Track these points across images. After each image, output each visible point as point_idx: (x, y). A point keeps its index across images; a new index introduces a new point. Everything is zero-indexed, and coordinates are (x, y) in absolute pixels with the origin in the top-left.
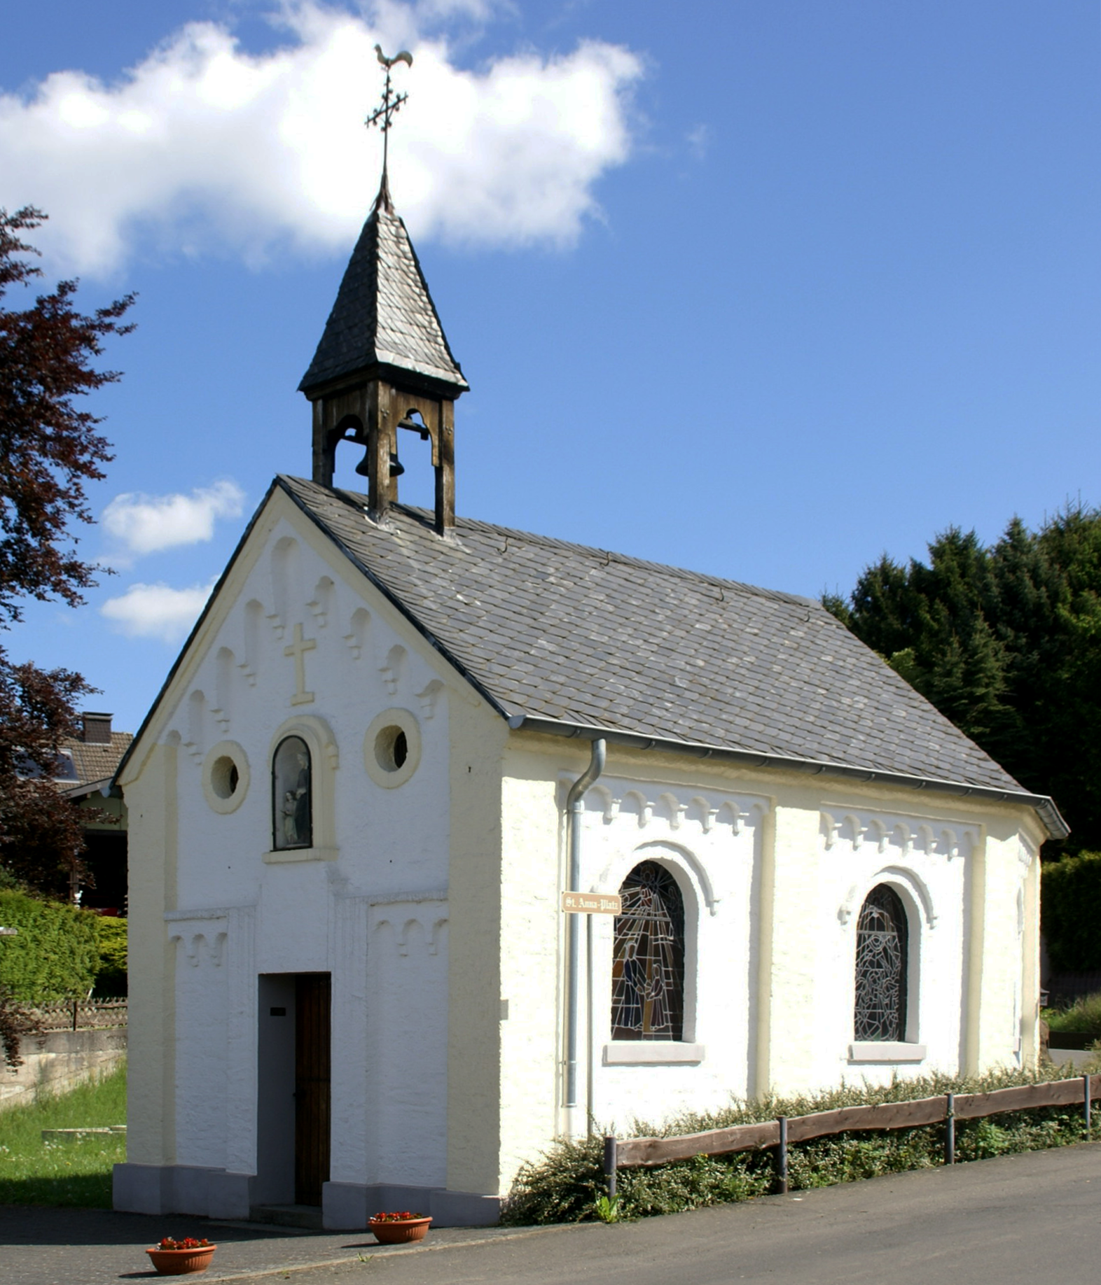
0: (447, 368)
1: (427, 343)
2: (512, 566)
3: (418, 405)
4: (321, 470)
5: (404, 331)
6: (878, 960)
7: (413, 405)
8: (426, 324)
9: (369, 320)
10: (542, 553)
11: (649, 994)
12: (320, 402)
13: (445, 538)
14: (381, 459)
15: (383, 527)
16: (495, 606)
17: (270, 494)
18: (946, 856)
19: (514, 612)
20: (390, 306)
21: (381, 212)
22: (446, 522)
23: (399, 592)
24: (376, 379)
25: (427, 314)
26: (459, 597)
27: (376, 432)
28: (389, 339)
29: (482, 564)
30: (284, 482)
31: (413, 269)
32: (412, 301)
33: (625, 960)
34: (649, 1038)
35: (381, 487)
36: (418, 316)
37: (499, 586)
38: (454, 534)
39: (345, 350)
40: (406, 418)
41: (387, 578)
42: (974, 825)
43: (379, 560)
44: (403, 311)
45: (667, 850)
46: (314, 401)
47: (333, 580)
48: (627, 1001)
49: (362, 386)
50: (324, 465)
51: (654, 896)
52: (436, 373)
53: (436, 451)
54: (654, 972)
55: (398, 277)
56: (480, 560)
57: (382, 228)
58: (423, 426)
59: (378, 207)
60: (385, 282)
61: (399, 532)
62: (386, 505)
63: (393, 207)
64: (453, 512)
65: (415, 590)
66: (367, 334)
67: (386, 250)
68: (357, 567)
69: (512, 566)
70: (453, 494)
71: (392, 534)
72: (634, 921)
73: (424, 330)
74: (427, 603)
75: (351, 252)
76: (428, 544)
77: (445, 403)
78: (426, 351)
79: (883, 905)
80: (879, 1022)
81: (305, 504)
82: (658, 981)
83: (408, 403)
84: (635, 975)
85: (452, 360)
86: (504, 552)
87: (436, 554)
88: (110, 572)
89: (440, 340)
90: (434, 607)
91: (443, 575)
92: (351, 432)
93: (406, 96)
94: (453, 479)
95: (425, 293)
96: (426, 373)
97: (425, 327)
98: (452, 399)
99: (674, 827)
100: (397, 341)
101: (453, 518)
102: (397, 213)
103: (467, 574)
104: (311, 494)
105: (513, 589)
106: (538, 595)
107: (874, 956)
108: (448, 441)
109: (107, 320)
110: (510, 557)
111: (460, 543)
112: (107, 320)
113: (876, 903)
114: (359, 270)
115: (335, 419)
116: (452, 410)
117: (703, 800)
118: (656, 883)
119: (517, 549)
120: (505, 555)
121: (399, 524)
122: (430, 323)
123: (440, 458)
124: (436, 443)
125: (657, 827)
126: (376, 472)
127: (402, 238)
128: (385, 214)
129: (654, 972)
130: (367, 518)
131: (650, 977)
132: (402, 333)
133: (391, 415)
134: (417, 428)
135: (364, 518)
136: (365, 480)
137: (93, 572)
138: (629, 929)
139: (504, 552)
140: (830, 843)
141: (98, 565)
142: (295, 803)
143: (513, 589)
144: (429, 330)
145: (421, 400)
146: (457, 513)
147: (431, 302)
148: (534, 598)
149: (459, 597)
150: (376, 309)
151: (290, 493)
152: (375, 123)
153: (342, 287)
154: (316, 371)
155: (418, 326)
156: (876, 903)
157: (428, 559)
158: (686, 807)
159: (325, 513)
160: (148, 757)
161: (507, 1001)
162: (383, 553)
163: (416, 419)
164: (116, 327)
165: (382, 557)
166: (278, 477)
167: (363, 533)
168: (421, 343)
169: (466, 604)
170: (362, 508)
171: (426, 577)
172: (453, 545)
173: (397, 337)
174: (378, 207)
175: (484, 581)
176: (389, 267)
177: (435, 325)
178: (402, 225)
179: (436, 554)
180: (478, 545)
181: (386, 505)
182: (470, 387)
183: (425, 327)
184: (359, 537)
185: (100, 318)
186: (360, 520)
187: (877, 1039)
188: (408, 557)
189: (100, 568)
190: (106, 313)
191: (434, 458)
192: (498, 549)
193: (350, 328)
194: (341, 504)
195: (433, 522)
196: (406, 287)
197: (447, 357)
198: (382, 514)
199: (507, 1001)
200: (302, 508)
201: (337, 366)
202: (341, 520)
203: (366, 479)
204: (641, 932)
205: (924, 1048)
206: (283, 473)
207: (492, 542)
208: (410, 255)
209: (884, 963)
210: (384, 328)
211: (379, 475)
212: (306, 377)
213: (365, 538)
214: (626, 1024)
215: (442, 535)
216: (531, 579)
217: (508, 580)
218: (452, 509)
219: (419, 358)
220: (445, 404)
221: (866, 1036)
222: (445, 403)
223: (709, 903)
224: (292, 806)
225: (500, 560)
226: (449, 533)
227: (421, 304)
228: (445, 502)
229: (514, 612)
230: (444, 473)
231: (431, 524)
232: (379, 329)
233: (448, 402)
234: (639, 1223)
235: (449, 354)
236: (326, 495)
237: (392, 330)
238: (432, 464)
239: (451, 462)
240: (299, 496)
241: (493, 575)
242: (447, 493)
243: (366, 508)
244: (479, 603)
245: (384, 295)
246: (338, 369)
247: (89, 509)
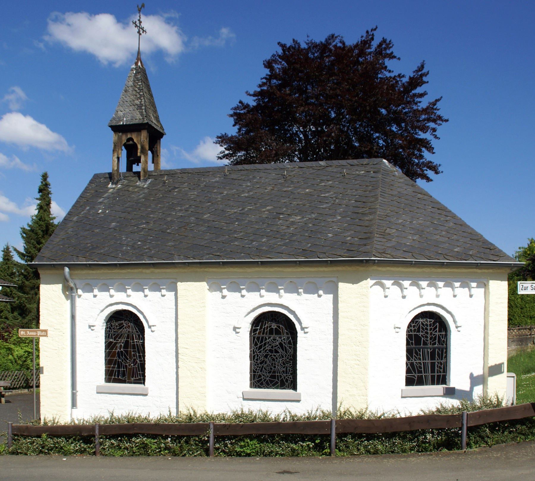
6: (275, 349)
11: (130, 365)
18: (316, 295)
33: (117, 351)
34: (130, 383)
42: (334, 277)
45: (435, 307)
48: (119, 367)
51: (131, 324)
54: (132, 355)
72: (122, 335)
79: (278, 321)
80: (278, 379)
82: (135, 360)
84: (122, 357)
99: (280, 297)
107: (272, 347)
113: (274, 321)
117: (468, 281)
118: (132, 319)
125: (120, 296)
129: (132, 355)
131: (130, 357)
138: (119, 338)
140: (455, 294)
156: (274, 321)
158: (225, 287)
161: (43, 367)
187: (277, 388)
199: (43, 367)
204: (125, 339)
205: (300, 394)
209: (280, 350)
214: (118, 376)
221: (269, 387)
223: (302, 329)
234: (107, 460)
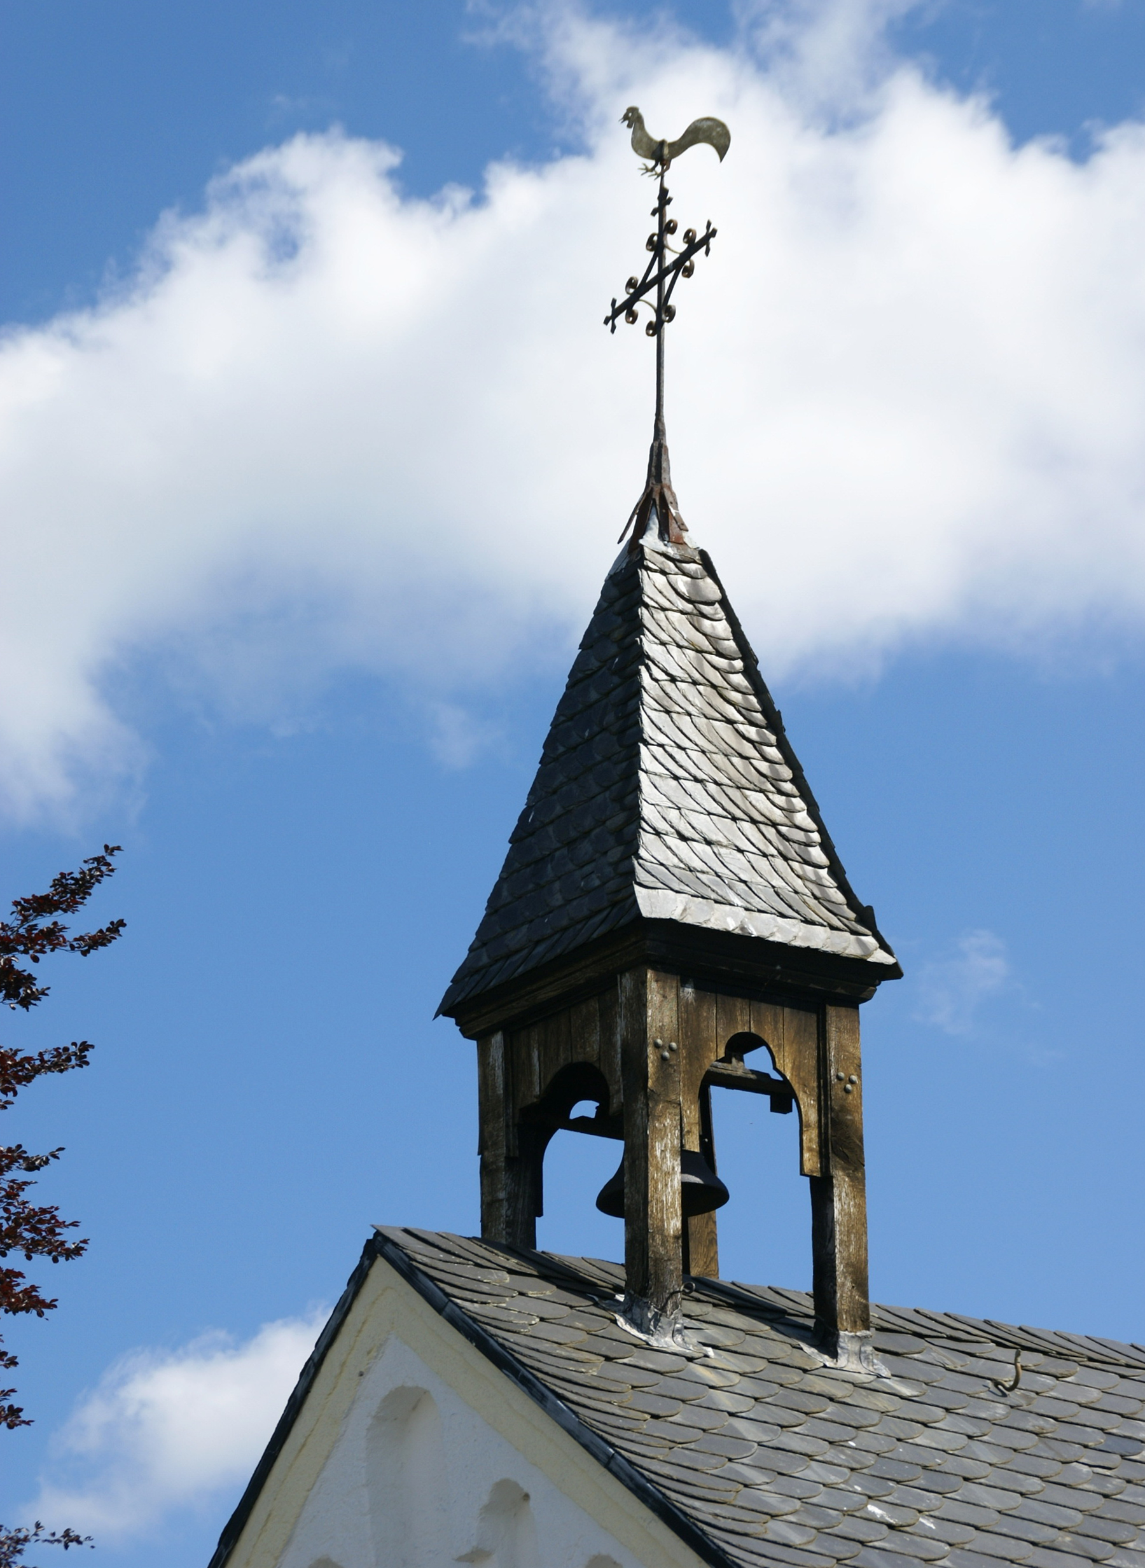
0: (835, 921)
1: (779, 862)
2: (1033, 1423)
3: (759, 1023)
4: (504, 1210)
5: (713, 836)
7: (744, 1024)
8: (778, 815)
9: (620, 818)
10: (1125, 1386)
12: (498, 1039)
13: (842, 1361)
14: (658, 1169)
15: (665, 1341)
16: (977, 1528)
17: (359, 1279)
19: (1034, 1544)
20: (676, 778)
21: (651, 541)
22: (844, 1321)
23: (697, 1504)
24: (637, 967)
25: (780, 792)
26: (874, 1509)
27: (642, 1098)
28: (671, 860)
29: (947, 1422)
30: (395, 1244)
31: (739, 679)
32: (736, 760)
35: (658, 1239)
36: (757, 798)
37: (994, 1476)
38: (869, 1349)
39: (558, 899)
40: (726, 1060)
41: (666, 1470)
43: (649, 1426)
44: (712, 787)
46: (480, 1036)
47: (526, 1488)
49: (605, 986)
50: (512, 1199)
52: (804, 938)
53: (812, 1137)
55: (698, 701)
56: (940, 1412)
57: (652, 584)
58: (775, 1076)
59: (641, 529)
60: (661, 718)
61: (710, 1351)
62: (674, 1283)
63: (682, 527)
64: (865, 1294)
65: (745, 1497)
66: (615, 854)
67: (664, 637)
68: (586, 1447)
69: (1033, 1423)
70: (862, 1247)
71: (690, 1359)
73: (770, 832)
74: (777, 1529)
75: (572, 651)
76: (794, 1377)
77: (832, 1012)
78: (778, 882)
81: (447, 1295)
83: (731, 1021)
85: (852, 901)
86: (1011, 1389)
87: (811, 1403)
88: (70, 1538)
89: (817, 854)
90: (796, 1538)
91: (830, 1454)
92: (585, 1109)
94: (861, 1208)
95: (773, 738)
96: (778, 938)
97: (774, 825)
98: (853, 1001)
100: (697, 864)
101: (866, 1308)
102: (695, 539)
103: (901, 1448)
104: (469, 1270)
105: (1034, 1484)
106: (1106, 1496)
108: (844, 1109)
109: (44, 922)
110: (1029, 1401)
111: (885, 1372)
112: (44, 922)
114: (594, 695)
115: (536, 1078)
116: (854, 1030)
119: (1050, 1381)
120: (1014, 1397)
121: (712, 1332)
122: (789, 811)
123: (824, 1155)
124: (812, 1116)
126: (646, 1202)
127: (710, 603)
128: (661, 546)
130: (621, 1321)
132: (709, 843)
133: (684, 1053)
134: (757, 1083)
135: (615, 1322)
136: (618, 1225)
137: (27, 1547)
139: (1011, 1389)
141: (38, 1526)
143: (1034, 1484)
144: (783, 829)
145: (767, 1010)
146: (874, 1299)
147: (790, 759)
148: (1096, 1503)
149: (874, 1509)
150: (638, 788)
151: (409, 1271)
153: (550, 744)
154: (485, 960)
155: (754, 821)
157: (787, 1417)
159: (502, 1315)
162: (660, 1407)
163: (757, 1061)
164: (70, 936)
165: (655, 1417)
166: (378, 1234)
167: (608, 1359)
168: (762, 864)
169: (891, 1527)
170: (612, 1298)
171: (781, 1461)
172: (863, 1378)
173: (694, 855)
174: (641, 529)
175: (950, 1464)
176: (673, 679)
177: (802, 818)
178: (710, 570)
179: (811, 1403)
180: (937, 1374)
181: (674, 1283)
182: (903, 967)
183: (774, 825)
184: (595, 1370)
185: (25, 919)
186: (598, 1324)
188: (731, 1414)
189: (44, 1534)
190: (42, 905)
191: (806, 1155)
192: (997, 1384)
193: (571, 844)
194: (549, 1290)
195: (810, 1323)
196: (721, 726)
197: (839, 897)
198: (663, 1309)
200: (439, 1309)
201: (538, 943)
202: (545, 1330)
203: (621, 1222)
206: (393, 1223)
207: (978, 1366)
208: (731, 645)
210: (658, 833)
211: (653, 1208)
212: (458, 979)
213: (612, 1370)
215: (834, 1355)
216: (1089, 1457)
217: (1020, 1462)
218: (861, 1284)
219: (757, 903)
220: (835, 1017)
222: (832, 1012)
225: (1000, 1410)
226: (853, 1346)
227: (764, 766)
228: (840, 1267)
229: (1034, 1544)
230: (836, 1191)
231: (806, 1328)
232: (647, 838)
233: (843, 1011)
235: (844, 887)
236: (511, 1272)
237: (683, 838)
238: (802, 1173)
239: (854, 1162)
240: (433, 1279)
241: (976, 1447)
242: (846, 1244)
243: (621, 1298)
244: (929, 1524)
245: (658, 751)
246: (540, 949)
247: (13, 1391)
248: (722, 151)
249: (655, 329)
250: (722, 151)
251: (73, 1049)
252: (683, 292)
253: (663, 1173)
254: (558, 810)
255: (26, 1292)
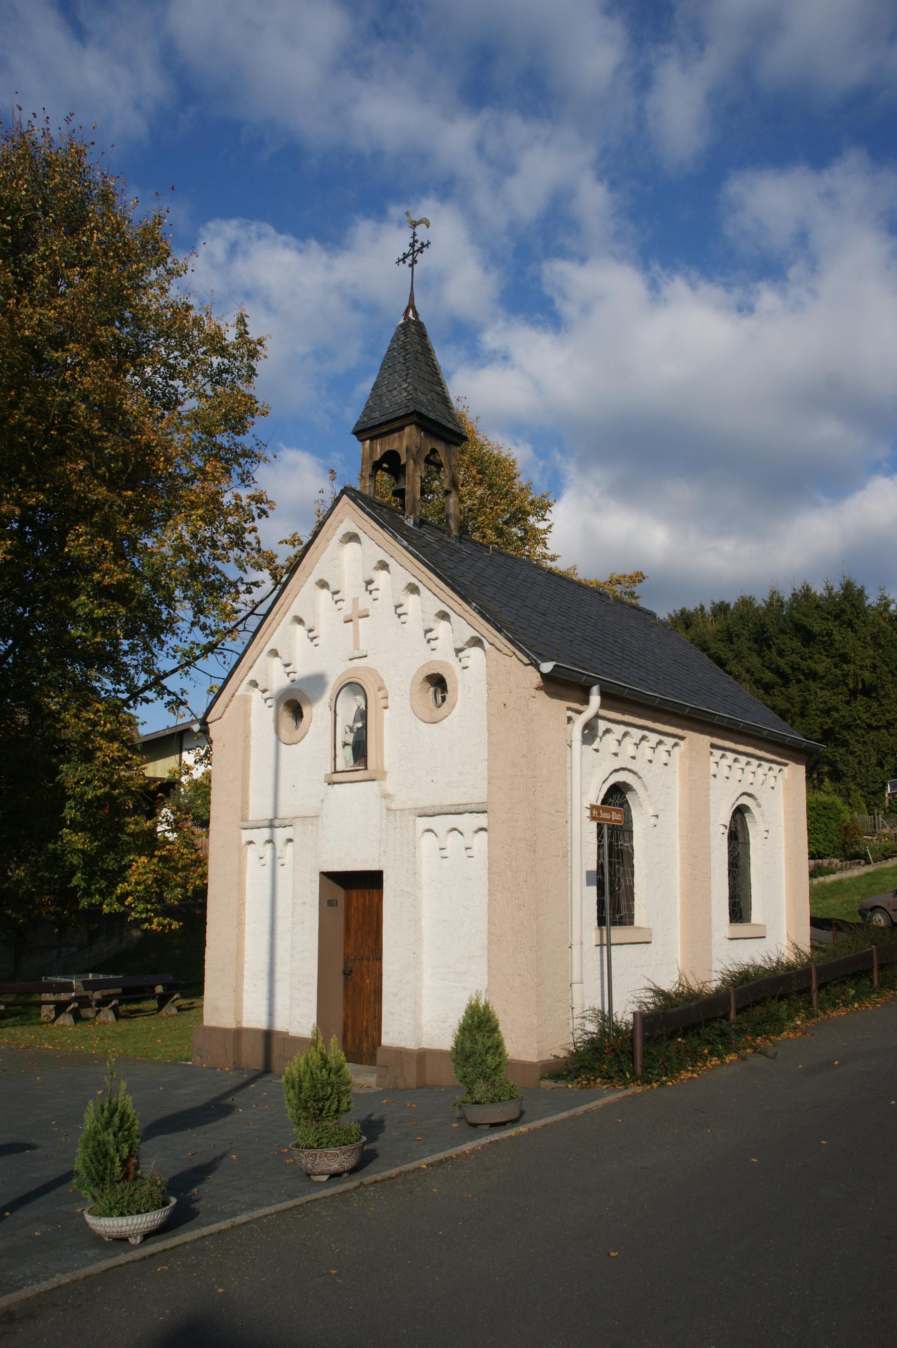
39: (388, 405)
93: (429, 243)
142: (352, 735)
152: (404, 262)
160: (264, 635)
224: (350, 738)
248: (428, 226)
249: (411, 265)
250: (428, 226)
251: (250, 419)
252: (419, 257)
253: (303, 1101)
254: (386, 382)
255: (869, 606)
